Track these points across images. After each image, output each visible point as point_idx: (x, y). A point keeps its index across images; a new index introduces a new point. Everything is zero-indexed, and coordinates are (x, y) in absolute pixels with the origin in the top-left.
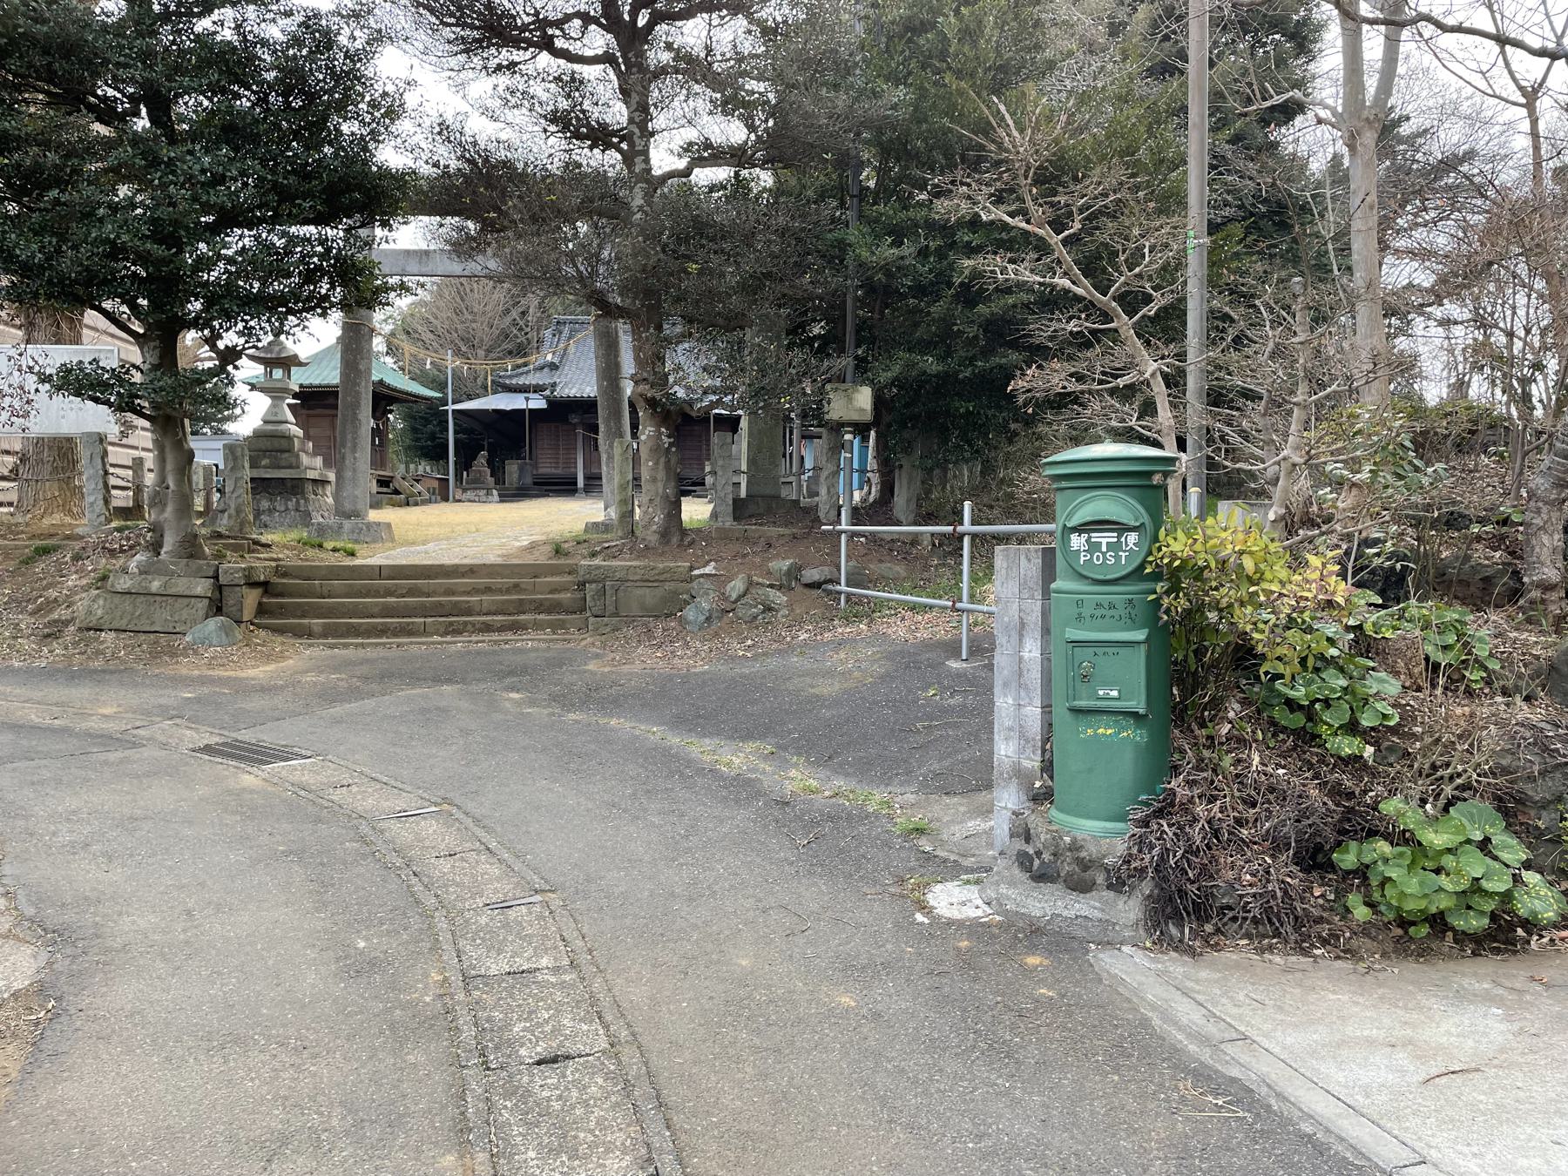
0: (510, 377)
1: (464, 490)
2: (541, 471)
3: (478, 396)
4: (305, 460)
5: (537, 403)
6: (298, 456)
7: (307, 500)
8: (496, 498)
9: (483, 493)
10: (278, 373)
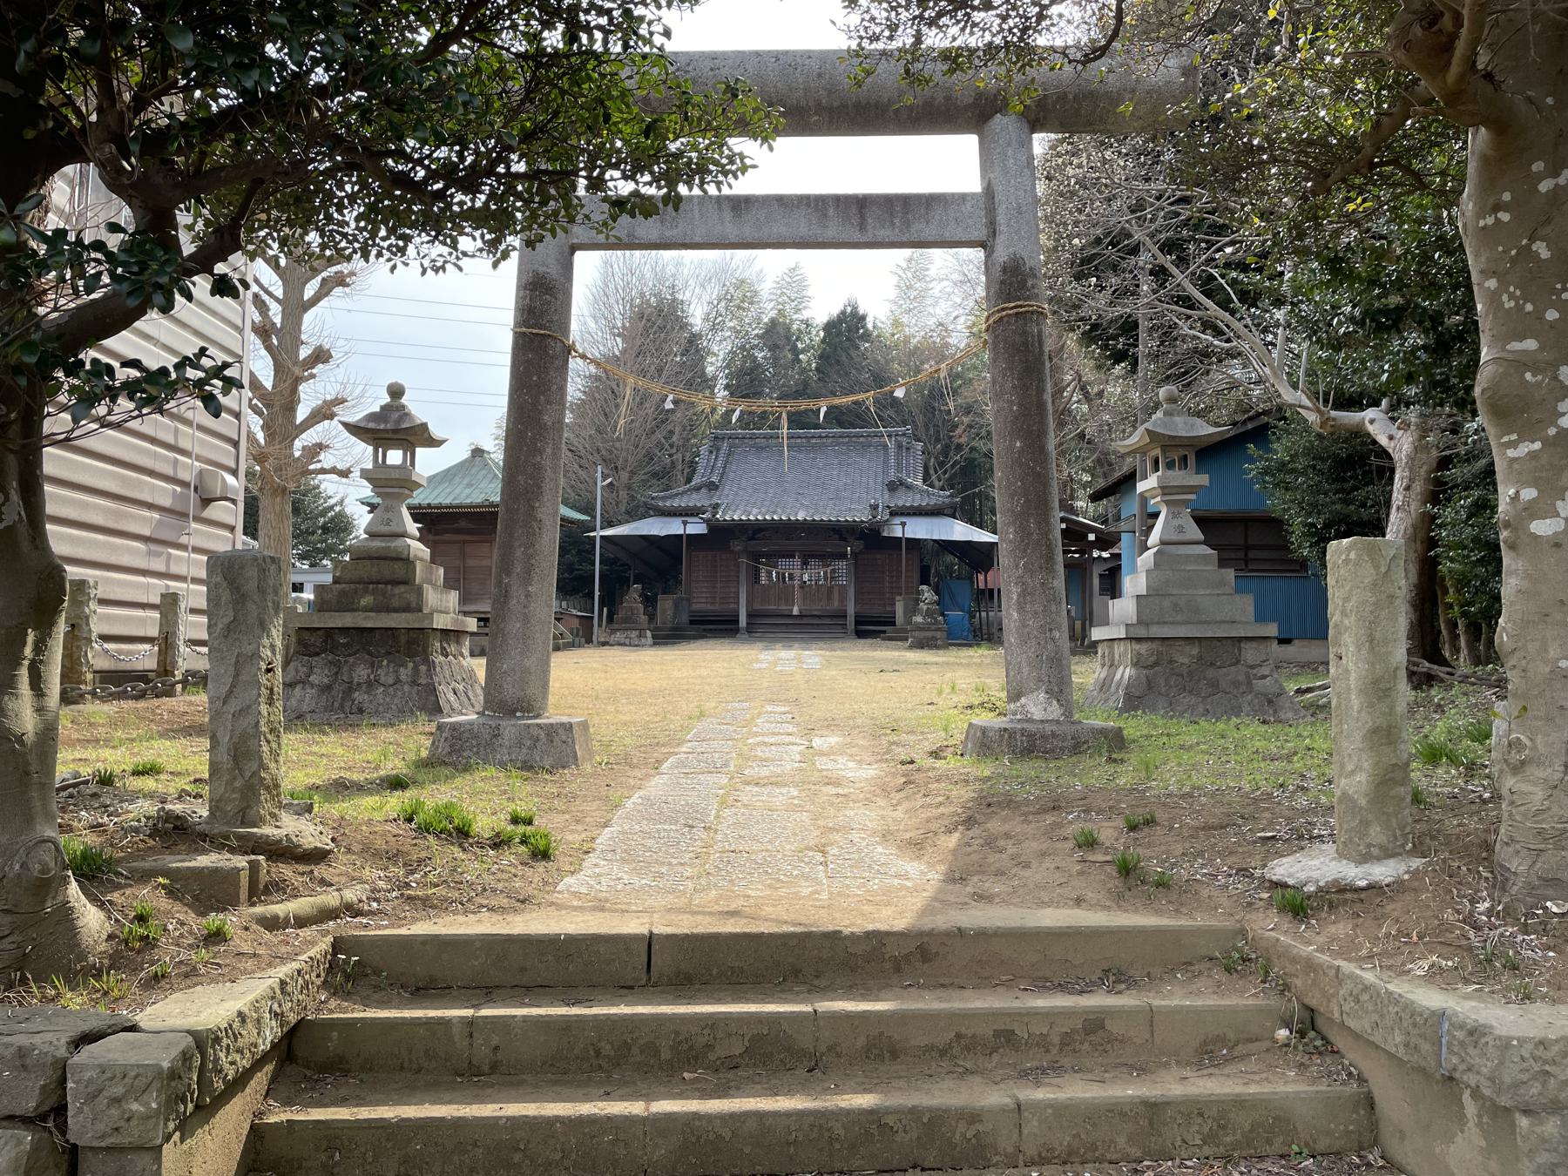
0: (664, 499)
1: (614, 631)
2: (695, 607)
3: (620, 523)
4: (432, 597)
5: (696, 528)
6: (419, 591)
7: (431, 666)
8: (650, 640)
9: (634, 634)
10: (395, 457)
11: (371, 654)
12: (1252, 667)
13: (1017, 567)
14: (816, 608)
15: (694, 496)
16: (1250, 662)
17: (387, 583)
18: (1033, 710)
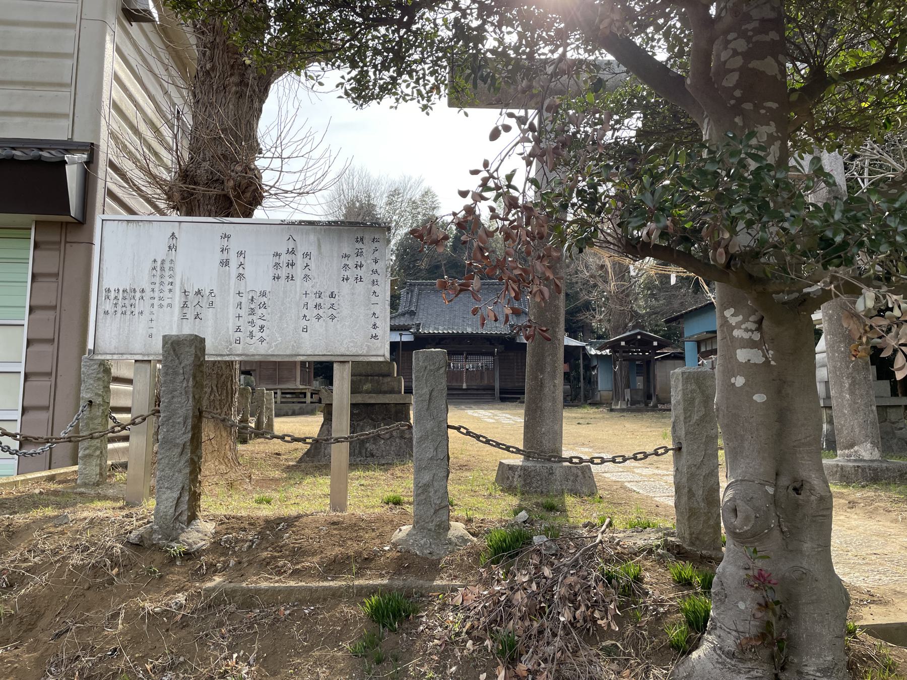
11: (372, 419)
12: (893, 423)
13: (848, 367)
14: (474, 384)
15: (402, 319)
16: (893, 420)
17: (378, 375)
18: (864, 454)
